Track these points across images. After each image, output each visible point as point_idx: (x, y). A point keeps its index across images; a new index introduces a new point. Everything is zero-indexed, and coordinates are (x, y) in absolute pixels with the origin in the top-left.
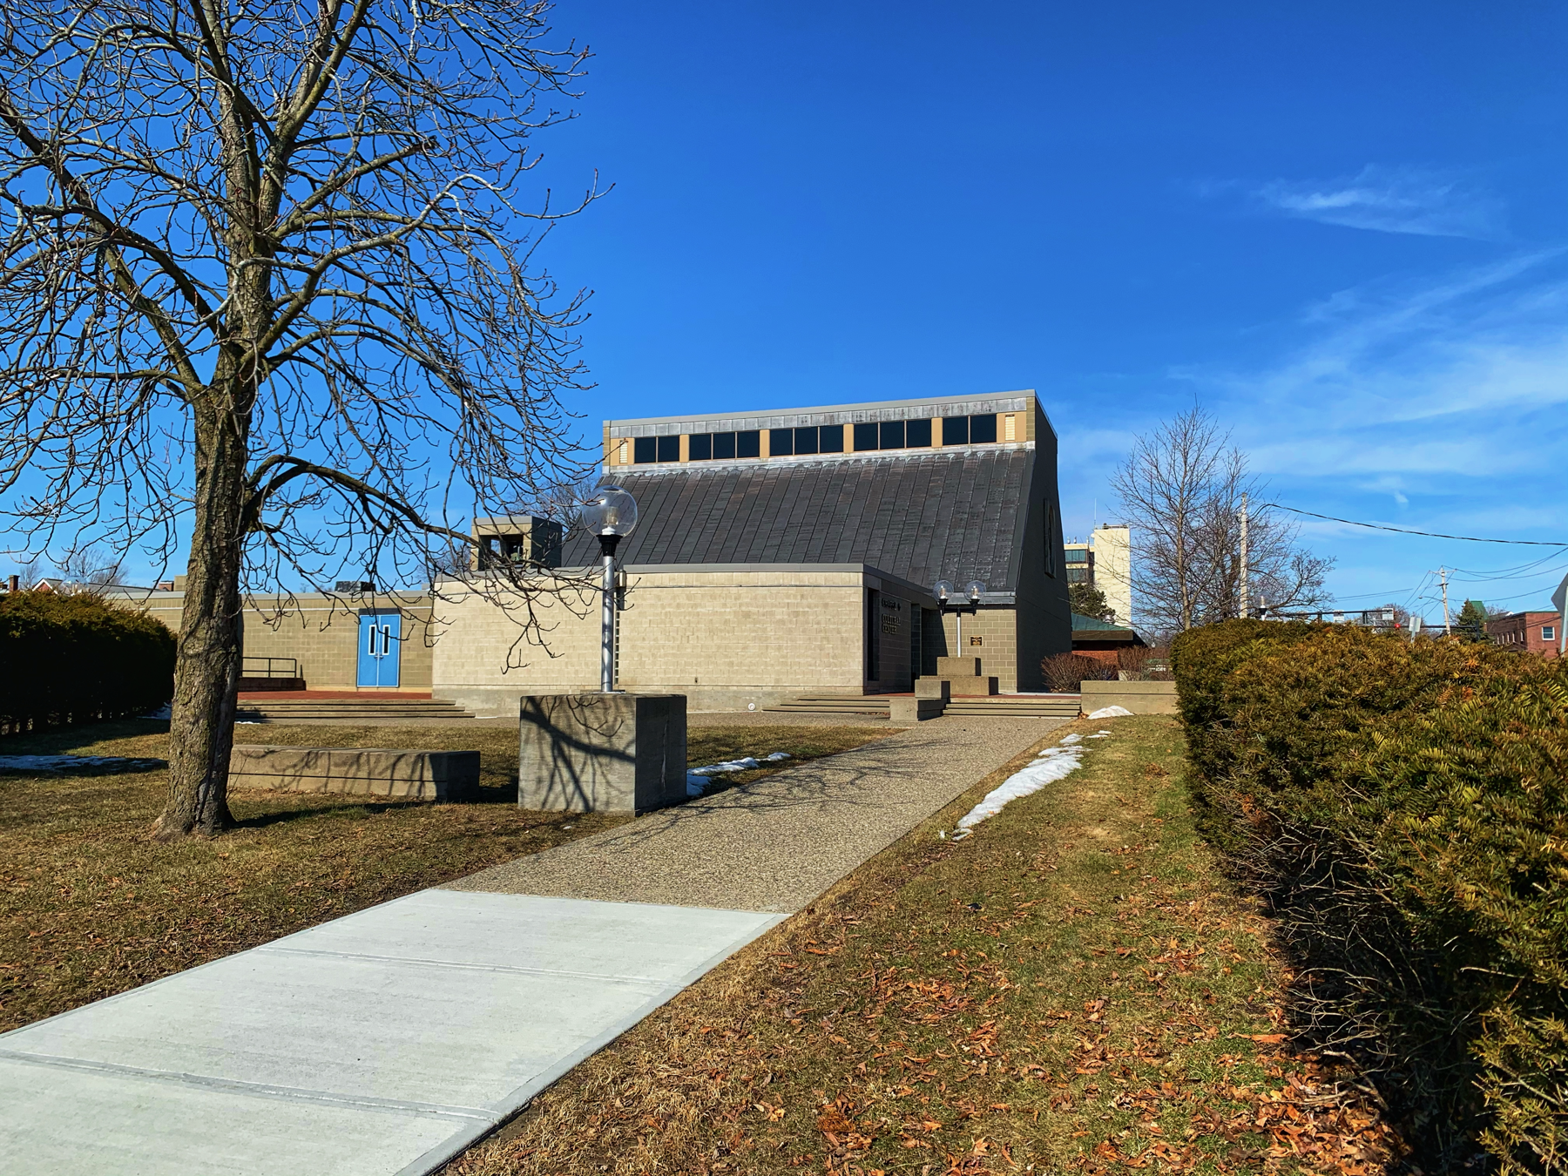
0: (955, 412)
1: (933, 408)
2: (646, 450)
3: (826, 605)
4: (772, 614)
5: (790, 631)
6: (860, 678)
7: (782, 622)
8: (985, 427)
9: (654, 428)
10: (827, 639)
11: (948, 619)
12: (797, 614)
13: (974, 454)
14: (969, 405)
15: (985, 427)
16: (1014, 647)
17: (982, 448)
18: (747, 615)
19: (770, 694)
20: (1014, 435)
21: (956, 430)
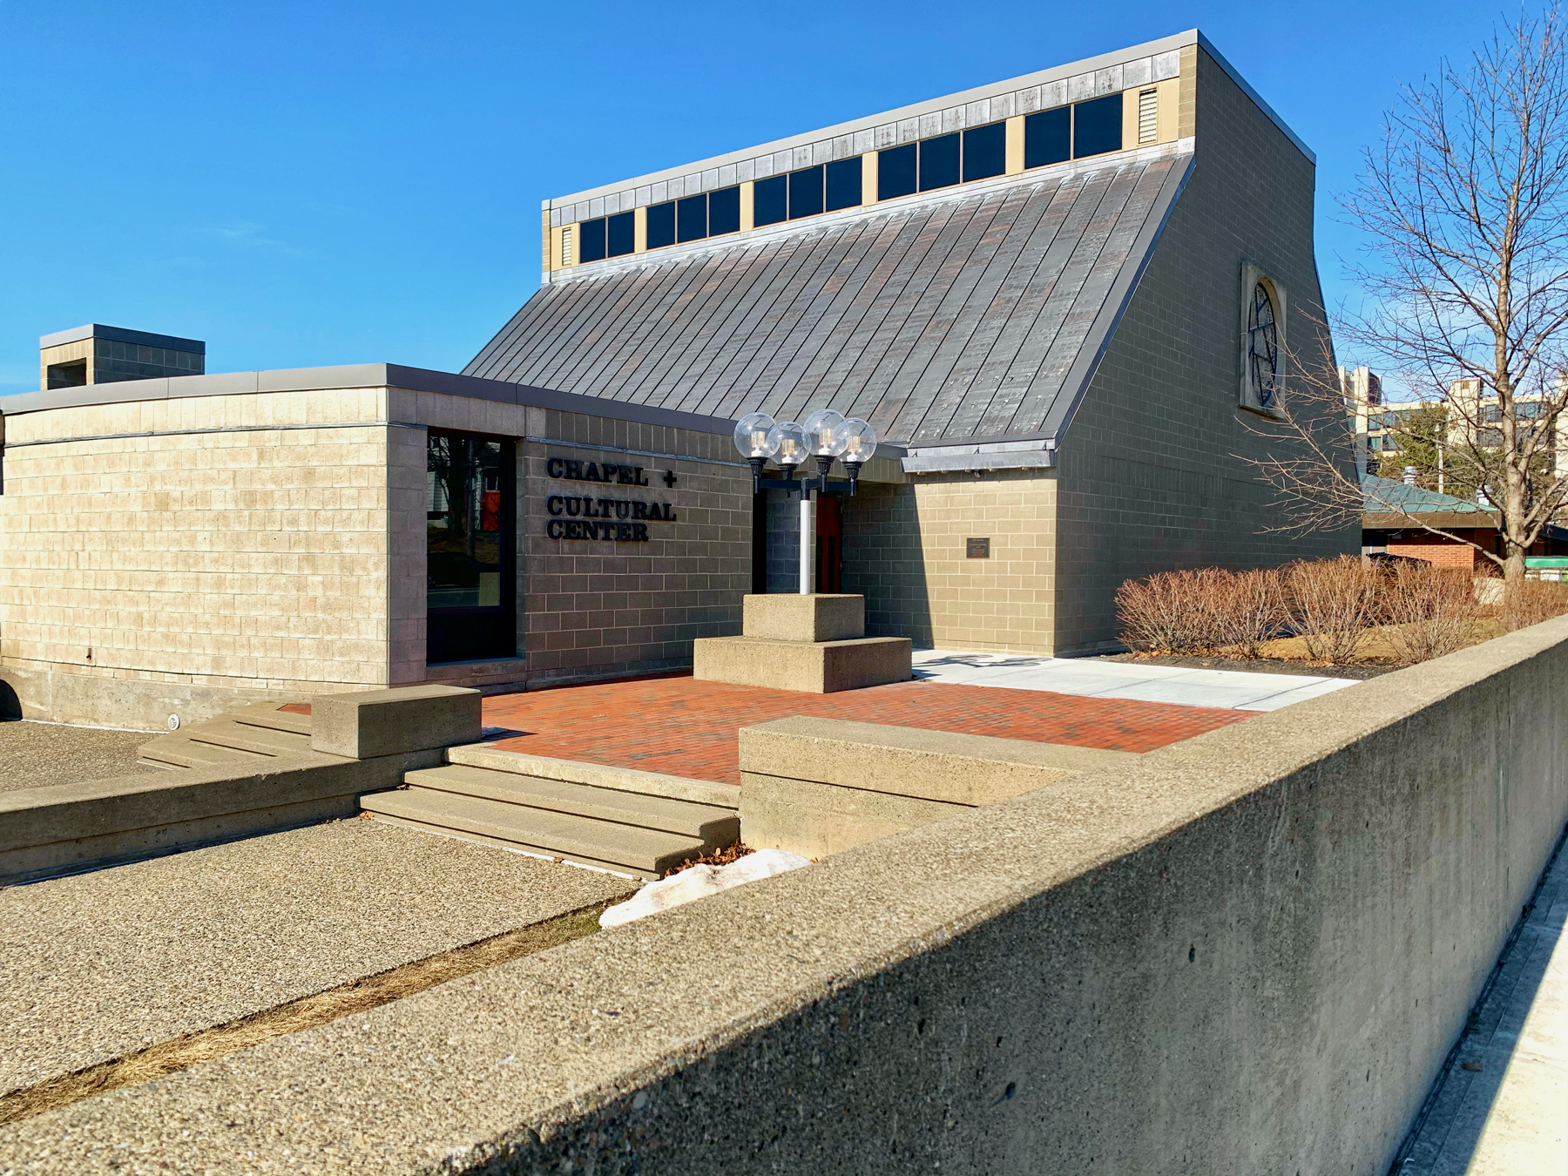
0: (1045, 101)
1: (1005, 102)
2: (605, 237)
3: (309, 474)
4: (204, 498)
5: (237, 539)
6: (382, 660)
7: (222, 517)
8: (1098, 123)
9: (601, 201)
10: (309, 559)
11: (921, 490)
12: (251, 498)
13: (1078, 177)
14: (1068, 84)
15: (1098, 123)
16: (1051, 561)
17: (1093, 165)
18: (163, 503)
19: (204, 695)
20: (1160, 132)
21: (1051, 136)
